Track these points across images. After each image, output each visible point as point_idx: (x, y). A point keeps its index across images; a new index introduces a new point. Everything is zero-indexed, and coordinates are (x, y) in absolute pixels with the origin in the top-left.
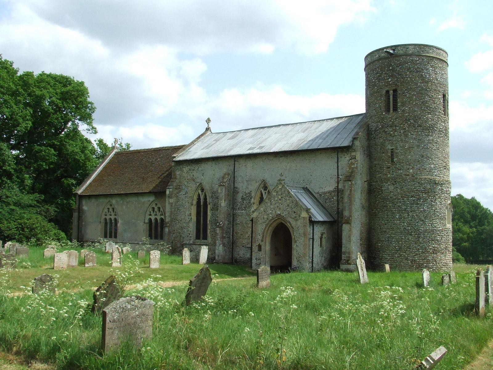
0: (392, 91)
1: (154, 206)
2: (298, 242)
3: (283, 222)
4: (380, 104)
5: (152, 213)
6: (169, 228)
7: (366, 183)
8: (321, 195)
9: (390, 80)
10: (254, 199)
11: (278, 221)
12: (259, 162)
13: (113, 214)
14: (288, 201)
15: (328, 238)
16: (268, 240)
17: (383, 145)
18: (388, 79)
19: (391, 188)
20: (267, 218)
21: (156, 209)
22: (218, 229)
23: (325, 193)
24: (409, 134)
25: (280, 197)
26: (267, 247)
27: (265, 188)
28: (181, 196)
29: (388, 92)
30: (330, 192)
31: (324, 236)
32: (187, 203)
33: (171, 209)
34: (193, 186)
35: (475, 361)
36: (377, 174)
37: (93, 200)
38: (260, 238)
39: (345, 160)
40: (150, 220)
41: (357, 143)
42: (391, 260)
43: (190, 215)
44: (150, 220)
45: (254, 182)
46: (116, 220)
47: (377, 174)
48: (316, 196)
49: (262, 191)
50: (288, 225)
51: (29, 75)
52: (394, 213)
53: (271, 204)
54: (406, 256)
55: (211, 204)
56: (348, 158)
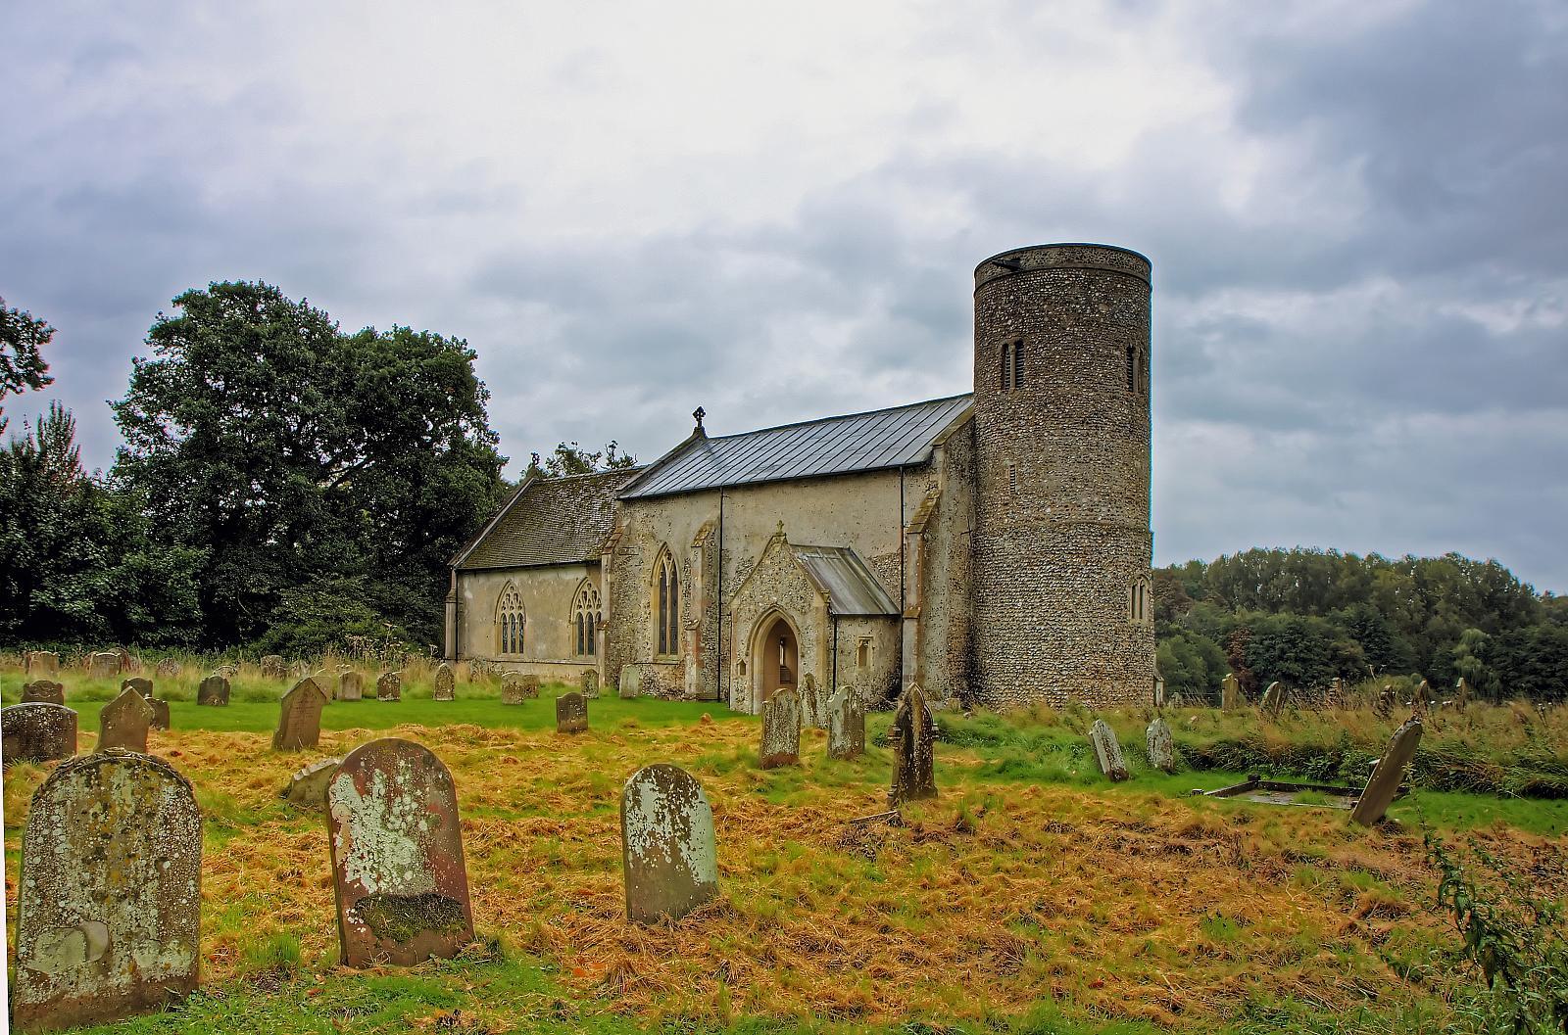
0: (1013, 347)
1: (586, 589)
6: (606, 633)
8: (875, 563)
13: (516, 605)
15: (1210, 652)
16: (758, 651)
21: (589, 595)
23: (883, 558)
24: (1046, 434)
25: (777, 569)
28: (630, 569)
29: (1006, 346)
31: (870, 645)
32: (642, 583)
33: (612, 593)
34: (653, 549)
35: (530, 826)
37: (482, 579)
38: (743, 648)
41: (939, 456)
42: (1007, 691)
44: (580, 615)
45: (759, 538)
46: (521, 617)
50: (790, 622)
54: (1036, 683)
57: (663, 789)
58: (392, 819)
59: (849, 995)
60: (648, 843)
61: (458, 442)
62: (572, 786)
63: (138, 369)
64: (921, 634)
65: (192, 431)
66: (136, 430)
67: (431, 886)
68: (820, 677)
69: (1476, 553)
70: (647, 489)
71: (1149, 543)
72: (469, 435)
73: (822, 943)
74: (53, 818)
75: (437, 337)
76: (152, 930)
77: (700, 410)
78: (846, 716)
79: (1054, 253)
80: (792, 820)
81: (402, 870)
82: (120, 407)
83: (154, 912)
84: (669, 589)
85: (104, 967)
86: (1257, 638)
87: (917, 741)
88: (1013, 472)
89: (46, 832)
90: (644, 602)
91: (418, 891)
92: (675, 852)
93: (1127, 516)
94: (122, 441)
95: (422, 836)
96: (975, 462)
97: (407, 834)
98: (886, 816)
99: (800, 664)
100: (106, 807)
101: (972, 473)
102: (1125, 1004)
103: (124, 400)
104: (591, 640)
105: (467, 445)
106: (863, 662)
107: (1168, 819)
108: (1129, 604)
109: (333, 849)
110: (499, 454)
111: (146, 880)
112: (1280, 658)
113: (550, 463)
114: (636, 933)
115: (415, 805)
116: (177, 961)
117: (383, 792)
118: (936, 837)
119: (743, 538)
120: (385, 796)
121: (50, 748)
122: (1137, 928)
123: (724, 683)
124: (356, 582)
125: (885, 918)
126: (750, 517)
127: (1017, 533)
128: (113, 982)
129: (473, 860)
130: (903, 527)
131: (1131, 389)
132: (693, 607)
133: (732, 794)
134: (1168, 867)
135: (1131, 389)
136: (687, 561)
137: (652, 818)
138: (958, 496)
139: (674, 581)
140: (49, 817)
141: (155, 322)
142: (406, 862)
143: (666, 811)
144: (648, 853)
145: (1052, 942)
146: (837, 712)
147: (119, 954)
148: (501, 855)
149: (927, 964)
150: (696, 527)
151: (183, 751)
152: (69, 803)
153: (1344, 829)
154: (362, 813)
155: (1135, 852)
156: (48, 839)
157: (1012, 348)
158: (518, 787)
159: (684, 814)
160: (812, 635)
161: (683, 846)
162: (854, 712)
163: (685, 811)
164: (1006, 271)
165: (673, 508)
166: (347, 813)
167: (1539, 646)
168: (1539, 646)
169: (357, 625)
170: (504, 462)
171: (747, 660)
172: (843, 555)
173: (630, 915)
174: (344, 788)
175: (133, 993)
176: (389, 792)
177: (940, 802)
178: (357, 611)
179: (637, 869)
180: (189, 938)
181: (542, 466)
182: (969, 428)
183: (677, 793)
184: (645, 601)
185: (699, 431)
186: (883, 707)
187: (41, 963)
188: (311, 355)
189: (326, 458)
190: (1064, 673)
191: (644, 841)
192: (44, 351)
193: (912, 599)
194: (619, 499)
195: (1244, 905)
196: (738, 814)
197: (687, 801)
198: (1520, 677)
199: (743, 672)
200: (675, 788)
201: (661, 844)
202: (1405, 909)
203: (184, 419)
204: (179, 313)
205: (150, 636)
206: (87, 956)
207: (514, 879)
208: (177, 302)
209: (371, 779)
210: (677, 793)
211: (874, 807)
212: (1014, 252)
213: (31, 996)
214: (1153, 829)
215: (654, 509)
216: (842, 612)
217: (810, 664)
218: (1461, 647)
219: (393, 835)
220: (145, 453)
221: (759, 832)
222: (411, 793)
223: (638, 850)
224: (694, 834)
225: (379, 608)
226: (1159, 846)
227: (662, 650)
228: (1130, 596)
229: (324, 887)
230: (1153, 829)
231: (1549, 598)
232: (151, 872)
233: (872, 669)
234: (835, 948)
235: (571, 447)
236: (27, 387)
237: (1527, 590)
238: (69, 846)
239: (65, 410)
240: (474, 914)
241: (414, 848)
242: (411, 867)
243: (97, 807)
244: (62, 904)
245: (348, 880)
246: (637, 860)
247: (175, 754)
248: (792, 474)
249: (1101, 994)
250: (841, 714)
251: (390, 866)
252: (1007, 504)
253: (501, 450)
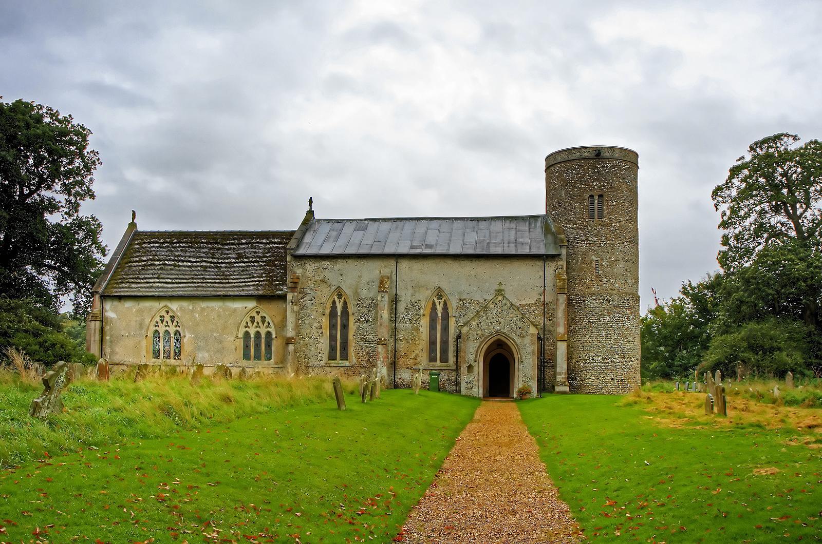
0: (597, 197)
1: (255, 314)
2: (524, 361)
3: (503, 338)
5: (250, 324)
9: (595, 184)
10: (425, 310)
12: (430, 265)
14: (511, 315)
17: (584, 255)
18: (593, 182)
19: (596, 303)
20: (482, 335)
22: (379, 346)
23: (524, 306)
24: (616, 245)
25: (499, 310)
26: (479, 368)
27: (440, 297)
32: (314, 313)
36: (577, 287)
40: (247, 334)
42: (596, 380)
43: (321, 327)
44: (247, 334)
46: (177, 333)
47: (577, 287)
49: (436, 300)
52: (599, 330)
53: (487, 318)
55: (356, 315)
79: (618, 151)
119: (411, 288)
127: (601, 296)
160: (529, 349)
190: (625, 370)
227: (332, 356)
252: (593, 281)
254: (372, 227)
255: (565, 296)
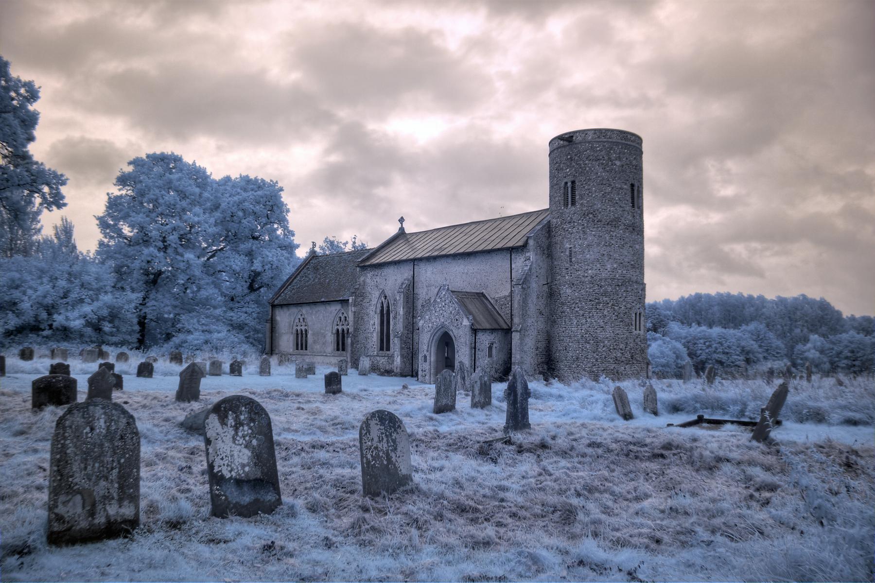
1: (341, 315)
4: (559, 198)
7: (546, 286)
8: (497, 301)
11: (442, 330)
16: (433, 350)
19: (569, 291)
21: (343, 319)
29: (566, 183)
30: (505, 297)
31: (495, 345)
33: (354, 318)
34: (376, 294)
37: (285, 309)
38: (425, 347)
39: (520, 263)
40: (338, 330)
41: (531, 242)
44: (338, 330)
46: (306, 331)
48: (492, 302)
50: (451, 333)
51: (227, 179)
56: (523, 260)
57: (382, 424)
58: (238, 438)
59: (483, 535)
60: (374, 453)
61: (273, 238)
62: (334, 422)
63: (110, 198)
64: (521, 339)
65: (136, 231)
66: (108, 231)
67: (259, 475)
68: (467, 362)
69: (815, 293)
70: (375, 261)
71: (644, 290)
72: (279, 232)
73: (468, 508)
74: (67, 434)
75: (263, 180)
76: (115, 495)
77: (402, 218)
78: (481, 384)
80: (452, 441)
81: (243, 466)
82: (99, 219)
83: (116, 485)
84: (385, 316)
85: (92, 514)
86: (702, 341)
87: (519, 398)
88: (570, 251)
89: (62, 442)
90: (372, 322)
91: (252, 477)
92: (389, 459)
93: (632, 274)
94: (100, 236)
95: (254, 448)
96: (550, 247)
97: (246, 447)
98: (502, 439)
99: (456, 356)
100: (92, 429)
101: (548, 251)
102: (630, 539)
103: (102, 215)
104: (343, 344)
105: (277, 237)
106: (490, 355)
107: (654, 440)
108: (634, 323)
109: (208, 454)
110: (296, 242)
111: (112, 469)
112: (715, 352)
113: (321, 248)
114: (368, 502)
115: (250, 431)
116: (127, 511)
117: (233, 424)
118: (529, 450)
120: (235, 426)
121: (64, 399)
122: (638, 499)
123: (415, 367)
124: (218, 312)
125: (501, 495)
126: (428, 275)
128: (96, 521)
129: (281, 461)
130: (512, 281)
131: (633, 206)
132: (397, 325)
133: (419, 427)
134: (654, 466)
135: (633, 206)
136: (395, 300)
137: (376, 439)
138: (541, 264)
139: (388, 311)
140: (64, 433)
141: (119, 174)
142: (245, 462)
143: (384, 435)
144: (374, 458)
145: (591, 506)
146: (476, 382)
147: (99, 507)
148: (295, 460)
149: (525, 519)
150: (399, 281)
151: (130, 401)
152: (73, 427)
153: (748, 444)
154: (222, 435)
155: (637, 457)
156: (63, 445)
157: (569, 184)
158: (304, 423)
159: (394, 437)
161: (393, 455)
162: (485, 382)
163: (394, 435)
164: (566, 143)
165: (389, 271)
166: (215, 435)
167: (849, 344)
168: (849, 344)
169: (220, 335)
170: (298, 246)
171: (427, 354)
172: (479, 297)
173: (364, 492)
174: (213, 421)
175: (106, 528)
176: (236, 424)
177: (532, 431)
178: (220, 328)
179: (368, 467)
180: (134, 499)
181: (317, 249)
182: (548, 230)
183: (390, 426)
184: (373, 322)
185: (402, 230)
186: (501, 380)
187: (61, 510)
188: (197, 190)
189: (204, 245)
191: (372, 452)
192: (63, 190)
193: (516, 320)
194: (358, 266)
195: (695, 485)
196: (423, 438)
197: (395, 430)
198: (840, 361)
199: (425, 361)
200: (389, 423)
201: (381, 454)
202: (779, 486)
203: (132, 226)
204: (130, 169)
205: (114, 339)
206: (84, 507)
207: (303, 472)
208: (130, 163)
209: (227, 417)
210: (390, 426)
211: (496, 434)
212: (570, 133)
213: (57, 527)
214: (646, 445)
215: (378, 272)
216: (479, 327)
217: (462, 356)
218: (809, 345)
219: (239, 447)
220: (112, 243)
221: (434, 448)
222: (248, 425)
223: (369, 456)
224: (399, 449)
225: (232, 325)
226: (649, 454)
228: (634, 318)
229: (203, 474)
230: (646, 445)
231: (853, 318)
232: (115, 464)
233: (495, 359)
234: (476, 510)
235: (332, 239)
236: (54, 208)
237: (839, 313)
238: (74, 449)
239: (68, 220)
240: (281, 490)
241: (250, 454)
242: (248, 465)
243: (88, 429)
244: (70, 479)
245: (215, 471)
246: (368, 462)
247: (126, 403)
248: (452, 252)
249: (618, 534)
250: (479, 383)
251: (237, 464)
253: (296, 240)
254: (506, 225)
255: (520, 287)
